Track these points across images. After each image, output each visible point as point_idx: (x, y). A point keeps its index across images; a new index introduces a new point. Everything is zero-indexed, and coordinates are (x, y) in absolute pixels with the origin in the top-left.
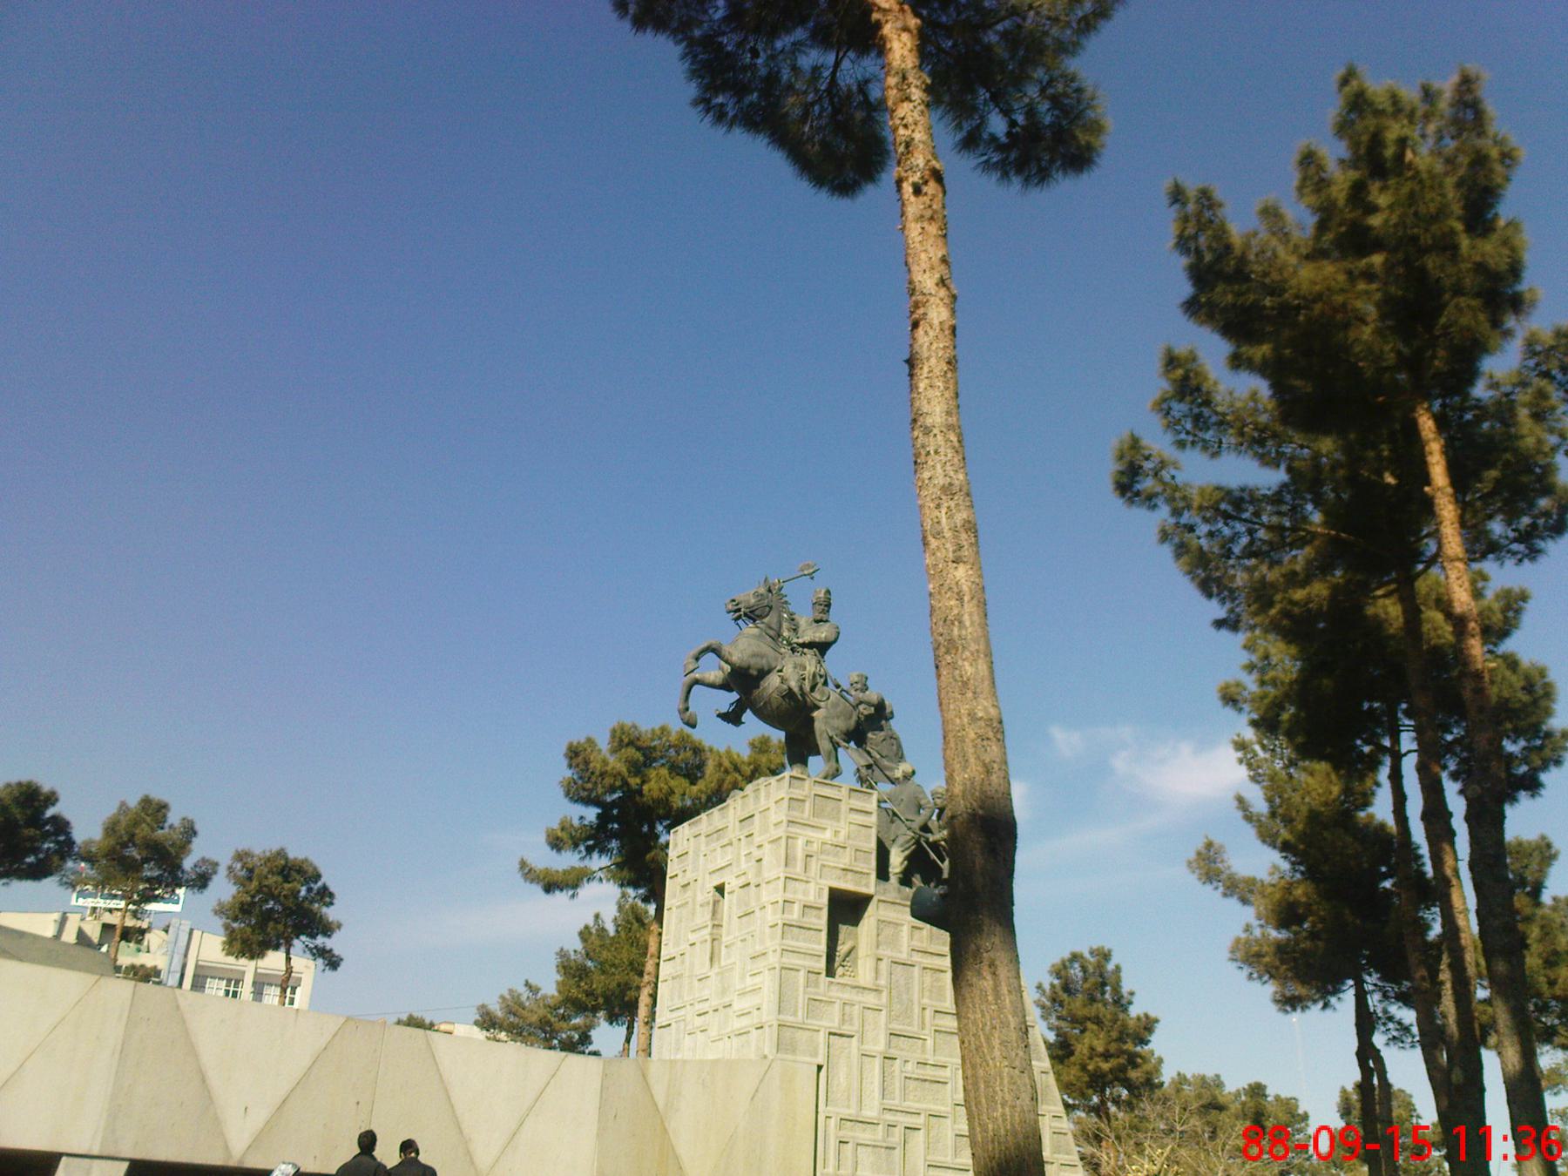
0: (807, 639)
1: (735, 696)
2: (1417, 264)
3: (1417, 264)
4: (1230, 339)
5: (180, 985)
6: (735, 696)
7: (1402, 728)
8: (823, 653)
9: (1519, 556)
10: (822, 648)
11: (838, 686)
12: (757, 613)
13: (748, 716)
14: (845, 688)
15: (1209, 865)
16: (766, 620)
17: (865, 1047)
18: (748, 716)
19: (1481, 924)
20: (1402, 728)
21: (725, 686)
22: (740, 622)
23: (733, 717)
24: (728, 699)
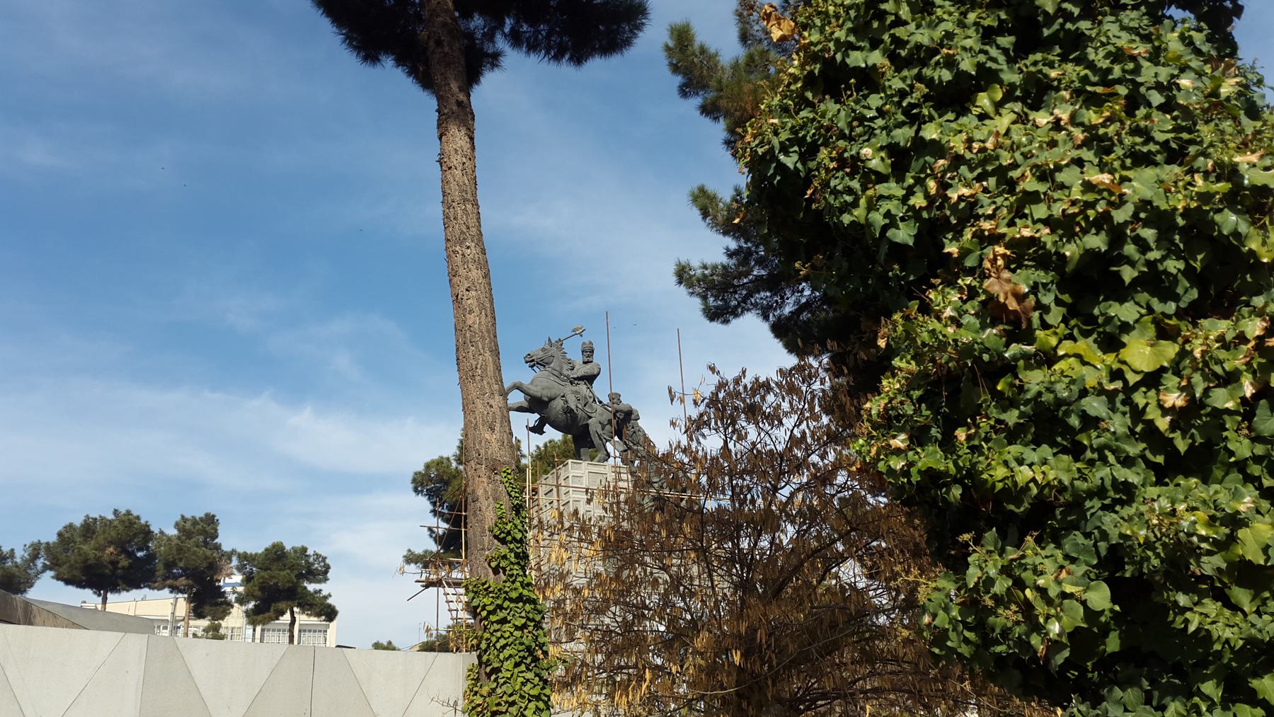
0: (580, 374)
1: (537, 416)
2: (846, 219)
3: (846, 219)
4: (593, 56)
5: (253, 640)
6: (537, 416)
7: (259, 629)
8: (591, 383)
9: (1240, 317)
10: (590, 379)
11: (600, 402)
12: (545, 361)
13: (547, 428)
14: (605, 403)
15: (428, 630)
16: (552, 365)
17: (961, 304)
18: (547, 428)
19: (1072, 214)
20: (259, 629)
21: (529, 410)
22: (535, 368)
23: (538, 429)
24: (533, 418)
